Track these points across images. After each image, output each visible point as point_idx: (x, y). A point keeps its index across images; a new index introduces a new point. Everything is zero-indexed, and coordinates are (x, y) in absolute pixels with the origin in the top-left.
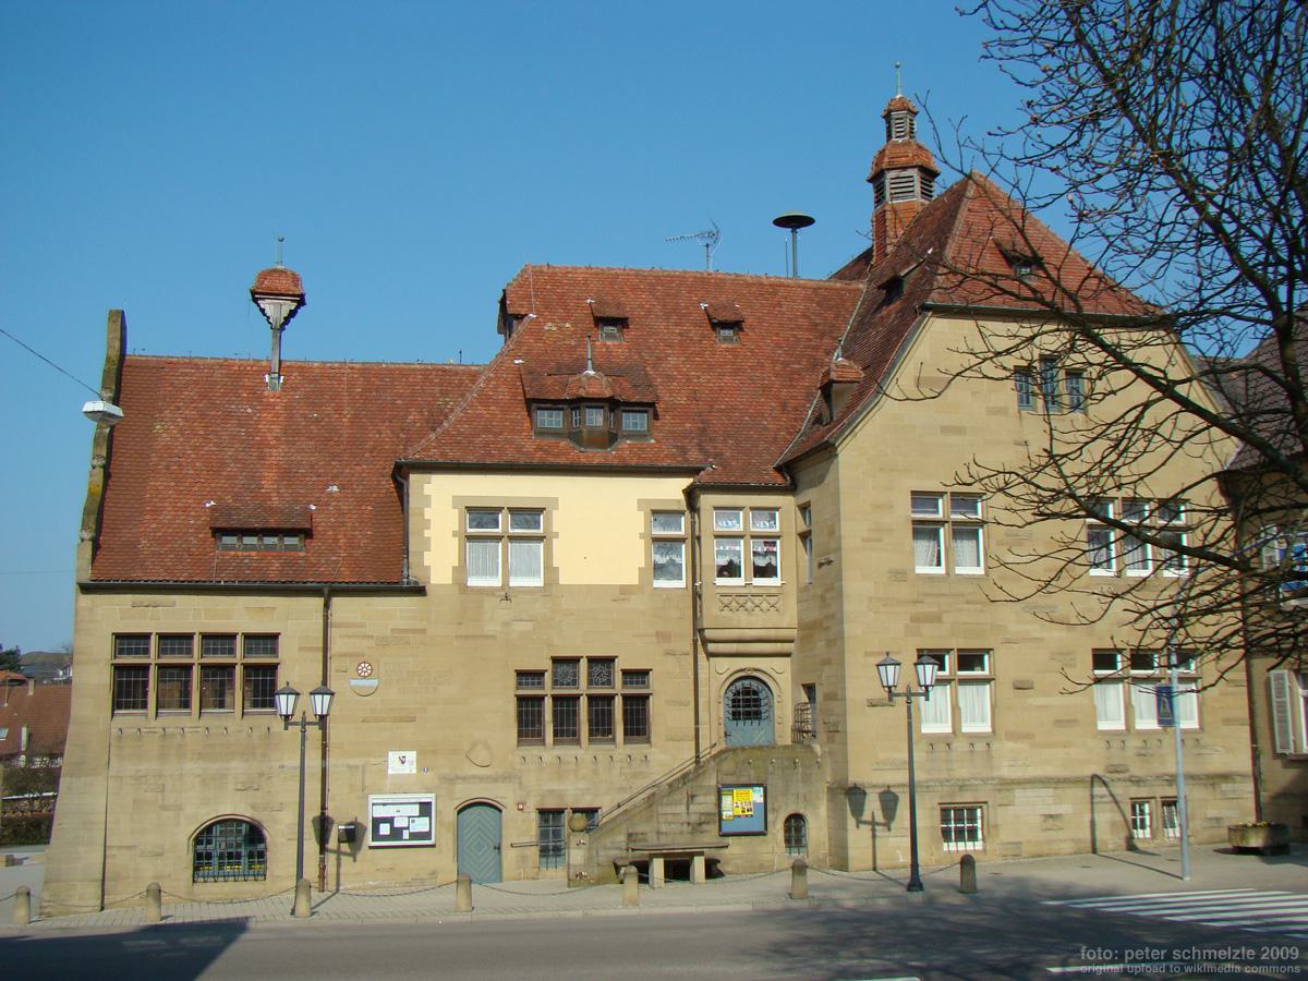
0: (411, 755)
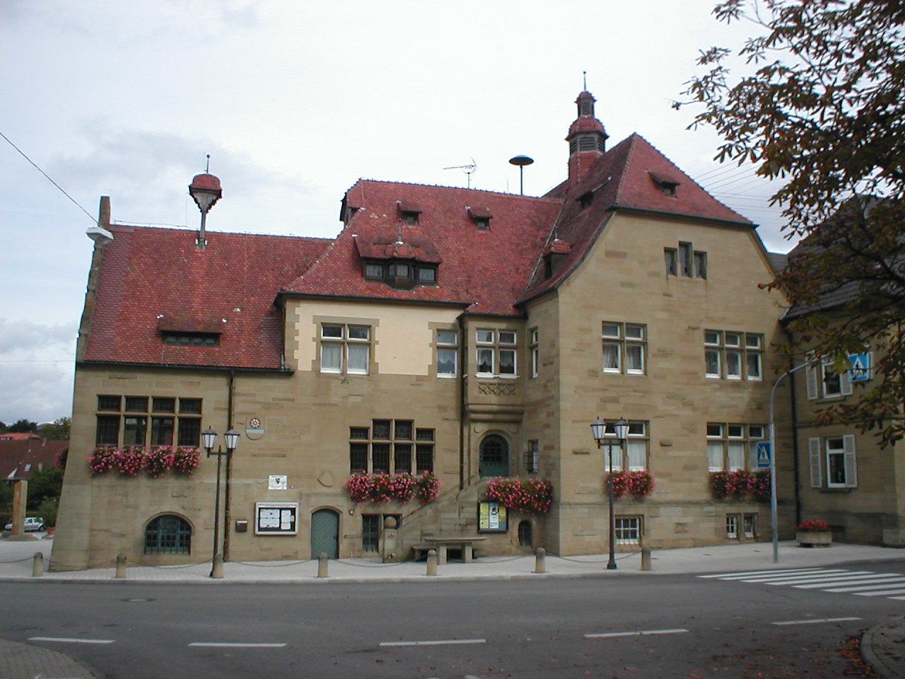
0: (284, 478)
